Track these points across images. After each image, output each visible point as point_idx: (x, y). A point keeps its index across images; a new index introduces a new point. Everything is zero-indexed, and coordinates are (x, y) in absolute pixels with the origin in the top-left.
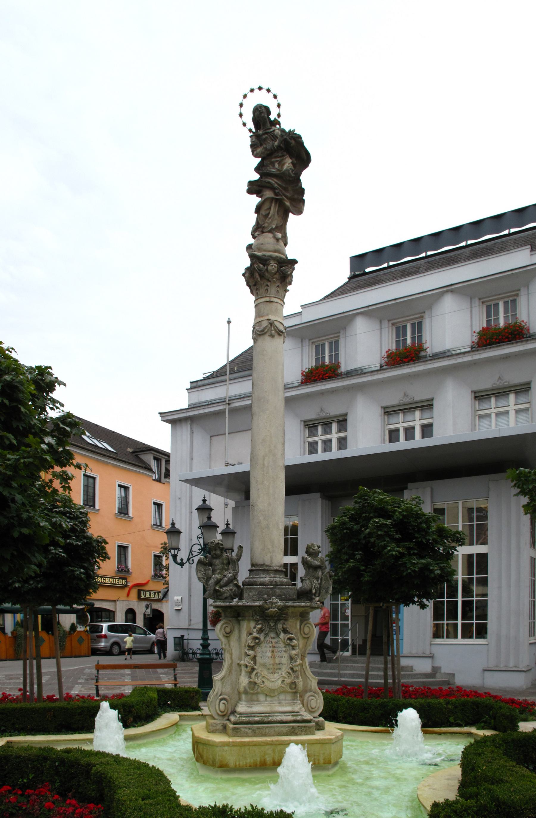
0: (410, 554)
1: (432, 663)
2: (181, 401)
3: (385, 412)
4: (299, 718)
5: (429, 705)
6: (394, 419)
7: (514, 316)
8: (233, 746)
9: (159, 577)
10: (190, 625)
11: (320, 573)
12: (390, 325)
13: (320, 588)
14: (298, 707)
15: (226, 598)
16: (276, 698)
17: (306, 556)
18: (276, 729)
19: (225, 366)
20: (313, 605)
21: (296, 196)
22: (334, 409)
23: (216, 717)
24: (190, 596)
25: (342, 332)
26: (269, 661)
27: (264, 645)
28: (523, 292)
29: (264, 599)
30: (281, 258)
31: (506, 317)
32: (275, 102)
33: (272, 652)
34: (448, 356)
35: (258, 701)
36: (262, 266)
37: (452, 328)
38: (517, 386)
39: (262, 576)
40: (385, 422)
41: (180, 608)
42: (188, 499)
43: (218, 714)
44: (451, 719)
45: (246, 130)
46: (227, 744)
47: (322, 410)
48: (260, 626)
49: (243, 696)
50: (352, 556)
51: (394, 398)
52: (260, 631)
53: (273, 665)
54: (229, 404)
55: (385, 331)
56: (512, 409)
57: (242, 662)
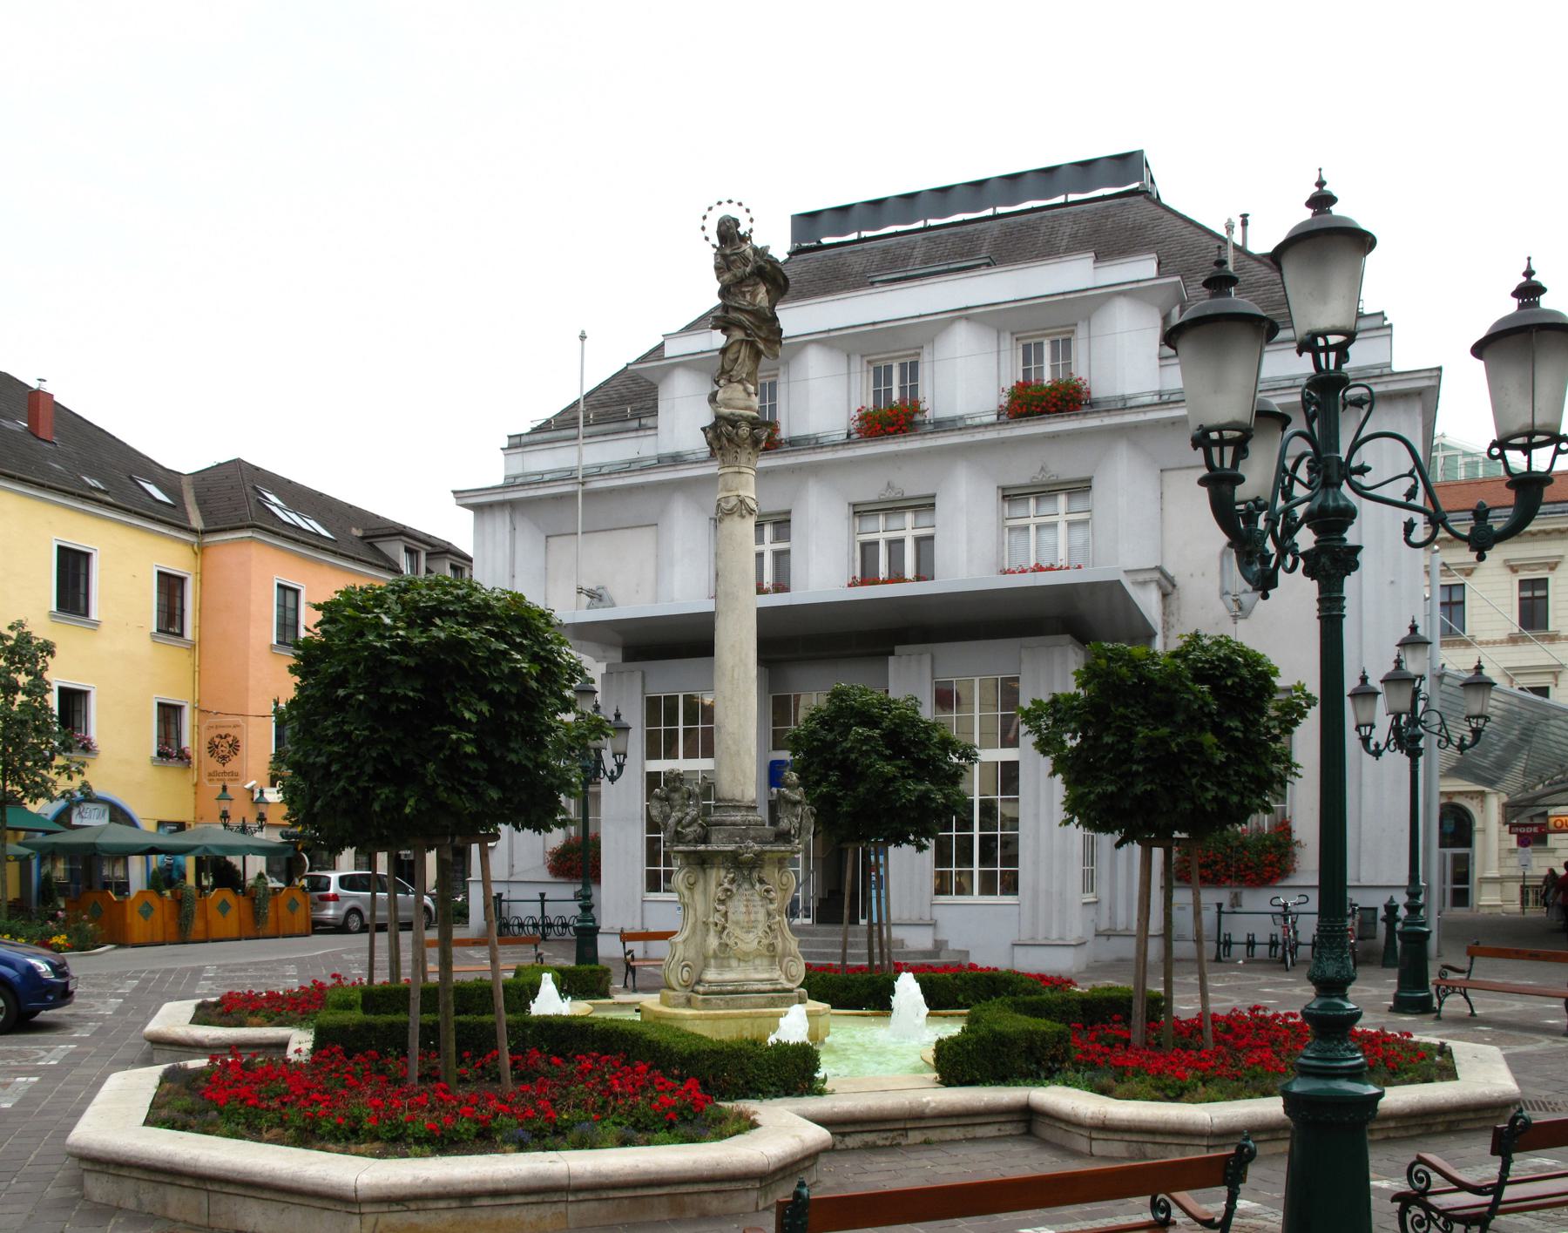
0: (904, 777)
2: (491, 471)
6: (869, 524)
7: (1068, 365)
25: (782, 369)
26: (742, 918)
27: (736, 898)
28: (1081, 332)
31: (1054, 368)
37: (966, 381)
44: (960, 998)
45: (708, 245)
46: (699, 1018)
49: (712, 962)
51: (869, 489)
52: (733, 881)
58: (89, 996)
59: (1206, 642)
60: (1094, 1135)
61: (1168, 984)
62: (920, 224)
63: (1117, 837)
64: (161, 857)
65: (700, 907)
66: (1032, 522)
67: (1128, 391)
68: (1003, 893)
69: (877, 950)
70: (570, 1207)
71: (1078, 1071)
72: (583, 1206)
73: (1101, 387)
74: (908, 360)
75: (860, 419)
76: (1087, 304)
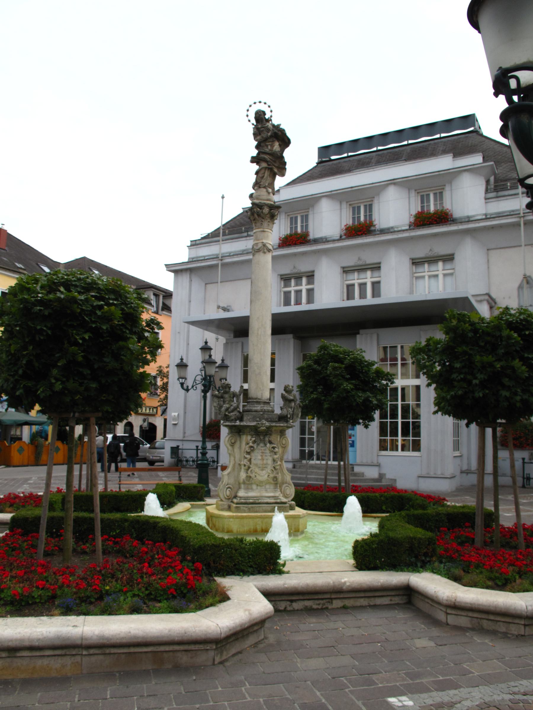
1: (379, 470)
2: (182, 256)
3: (344, 271)
4: (278, 501)
5: (368, 497)
6: (350, 276)
7: (442, 204)
8: (236, 518)
9: (154, 395)
10: (184, 437)
11: (293, 404)
12: (348, 206)
13: (293, 414)
14: (278, 494)
15: (232, 420)
16: (263, 487)
17: (284, 393)
18: (264, 508)
19: (219, 228)
20: (289, 425)
21: (281, 166)
22: (304, 267)
23: (224, 500)
24: (185, 413)
25: (310, 210)
26: (259, 462)
27: (256, 451)
28: (447, 188)
29: (257, 421)
30: (271, 205)
31: (435, 205)
32: (269, 109)
33: (262, 456)
34: (391, 232)
35: (252, 489)
36: (259, 209)
37: (394, 211)
38: (444, 256)
39: (256, 405)
40: (343, 278)
41: (176, 423)
42: (186, 333)
43: (225, 498)
44: (384, 508)
45: (250, 124)
46: (230, 517)
47: (294, 267)
48: (254, 439)
50: (315, 389)
51: (350, 260)
52: (254, 442)
53: (262, 465)
54: (221, 260)
55: (344, 211)
56: (440, 273)
57: (242, 463)
58: (40, 484)
59: (513, 312)
60: (449, 611)
61: (496, 506)
62: (375, 149)
63: (466, 421)
64: (37, 427)
65: (237, 456)
66: (426, 274)
67: (470, 214)
68: (413, 450)
69: (343, 478)
70: (84, 659)
71: (441, 562)
72: (93, 659)
73: (458, 212)
74: (368, 203)
75: (346, 229)
76: (449, 177)
